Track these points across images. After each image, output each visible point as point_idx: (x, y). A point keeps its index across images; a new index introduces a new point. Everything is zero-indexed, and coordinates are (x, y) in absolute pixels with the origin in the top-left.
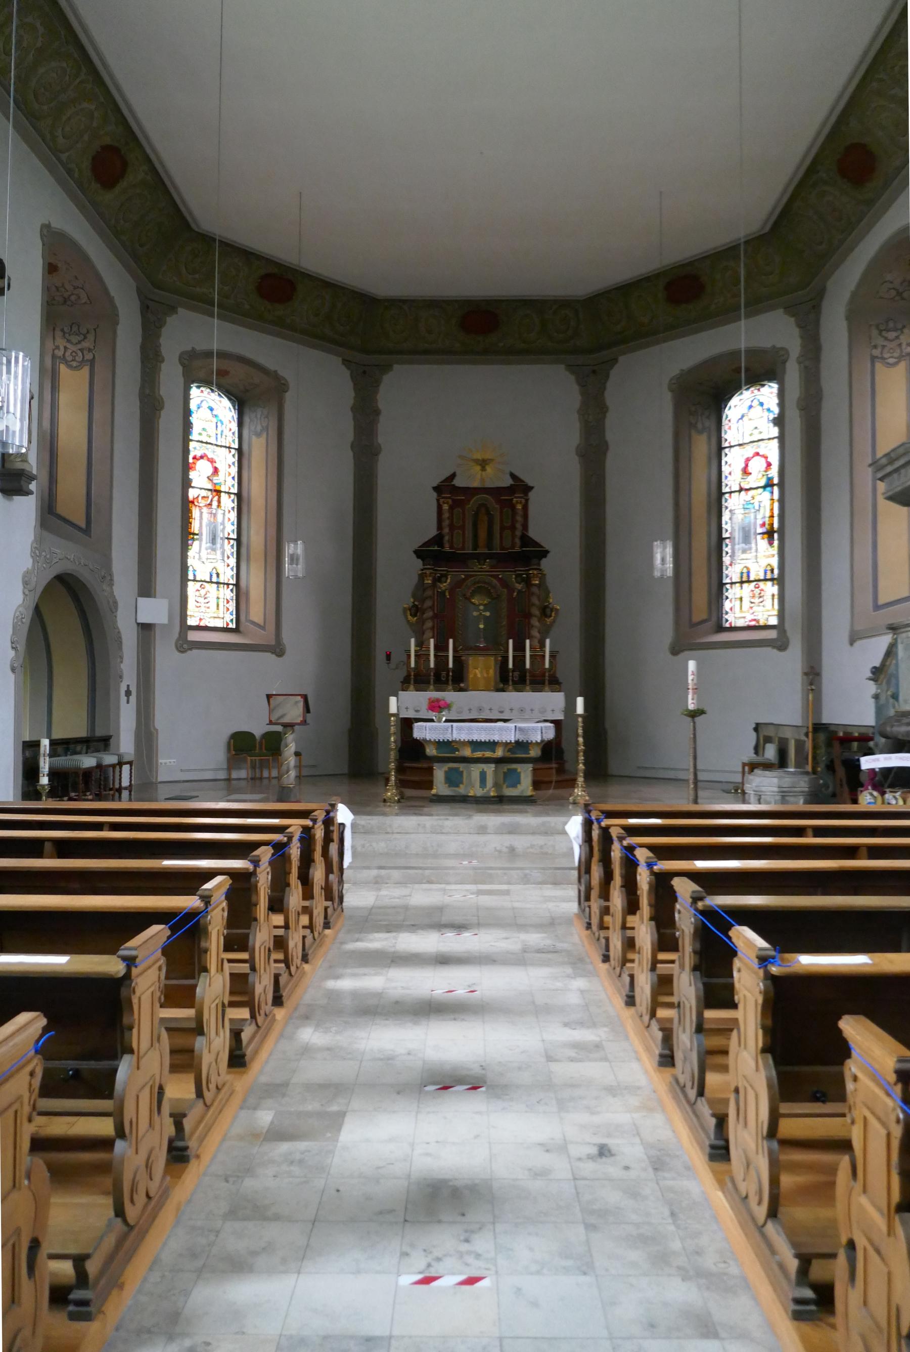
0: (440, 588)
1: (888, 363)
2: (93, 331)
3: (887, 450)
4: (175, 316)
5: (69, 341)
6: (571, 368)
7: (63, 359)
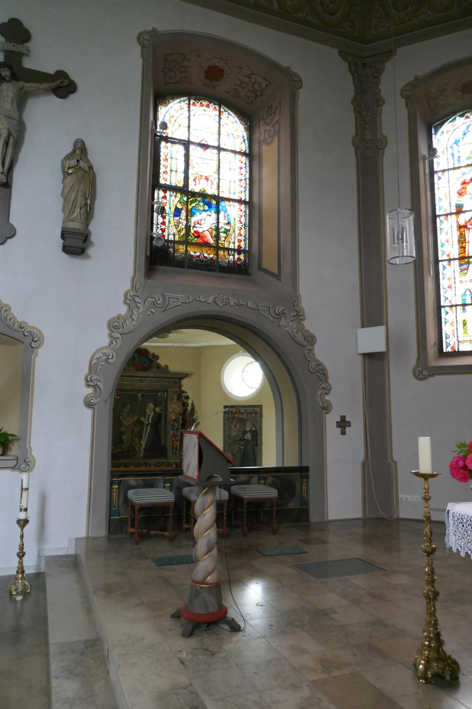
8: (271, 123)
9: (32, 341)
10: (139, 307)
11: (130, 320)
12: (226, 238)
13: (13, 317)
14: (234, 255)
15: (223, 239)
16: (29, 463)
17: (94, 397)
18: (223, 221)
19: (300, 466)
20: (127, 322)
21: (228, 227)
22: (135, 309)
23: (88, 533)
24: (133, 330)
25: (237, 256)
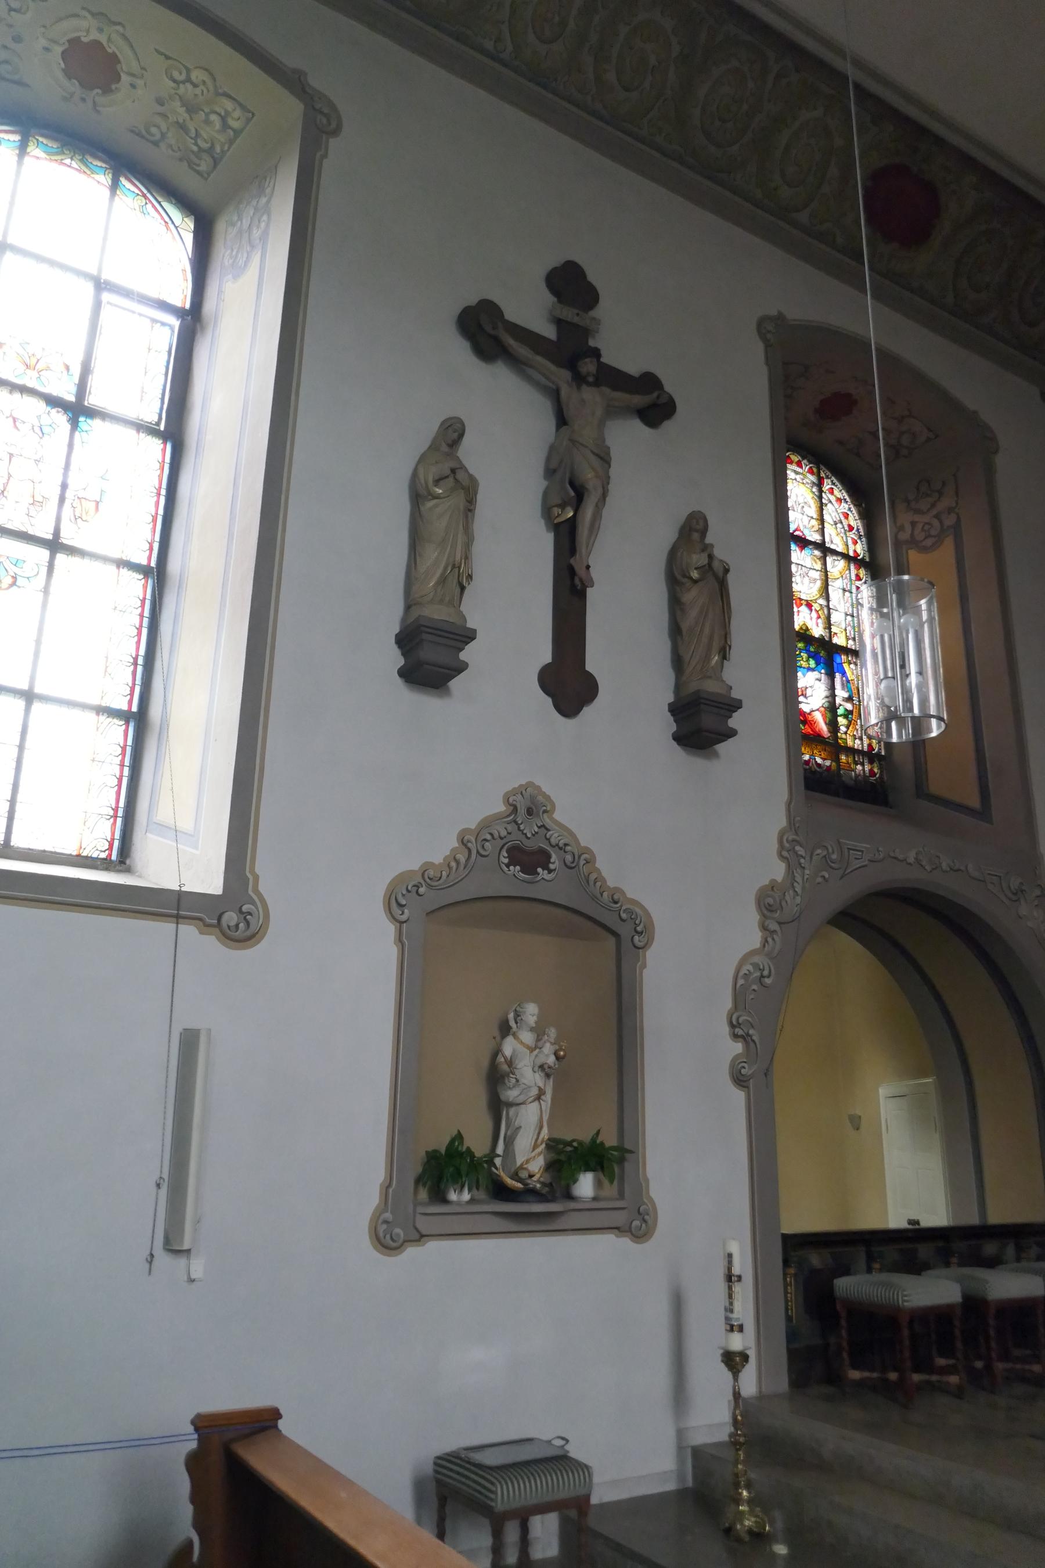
5: (918, 511)
7: (913, 543)
8: (928, 510)
9: (635, 934)
10: (803, 865)
11: (791, 892)
12: (848, 727)
13: (600, 878)
14: (863, 764)
15: (843, 729)
16: (646, 1217)
17: (745, 1062)
18: (841, 694)
19: (952, 1224)
20: (787, 898)
21: (849, 706)
22: (798, 870)
23: (760, 1388)
24: (797, 915)
25: (867, 768)
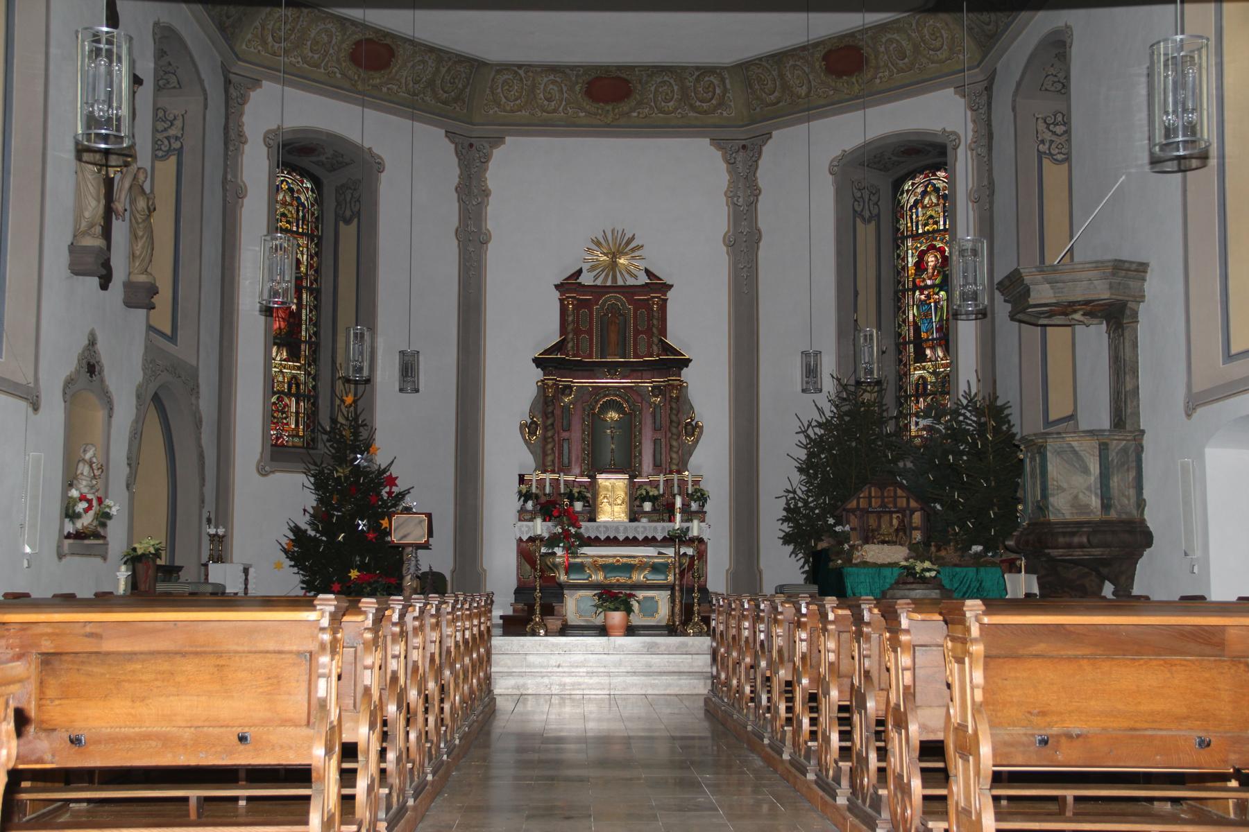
0: (564, 402)
1: (1056, 160)
2: (181, 117)
3: (1000, 279)
4: (258, 90)
6: (717, 143)
